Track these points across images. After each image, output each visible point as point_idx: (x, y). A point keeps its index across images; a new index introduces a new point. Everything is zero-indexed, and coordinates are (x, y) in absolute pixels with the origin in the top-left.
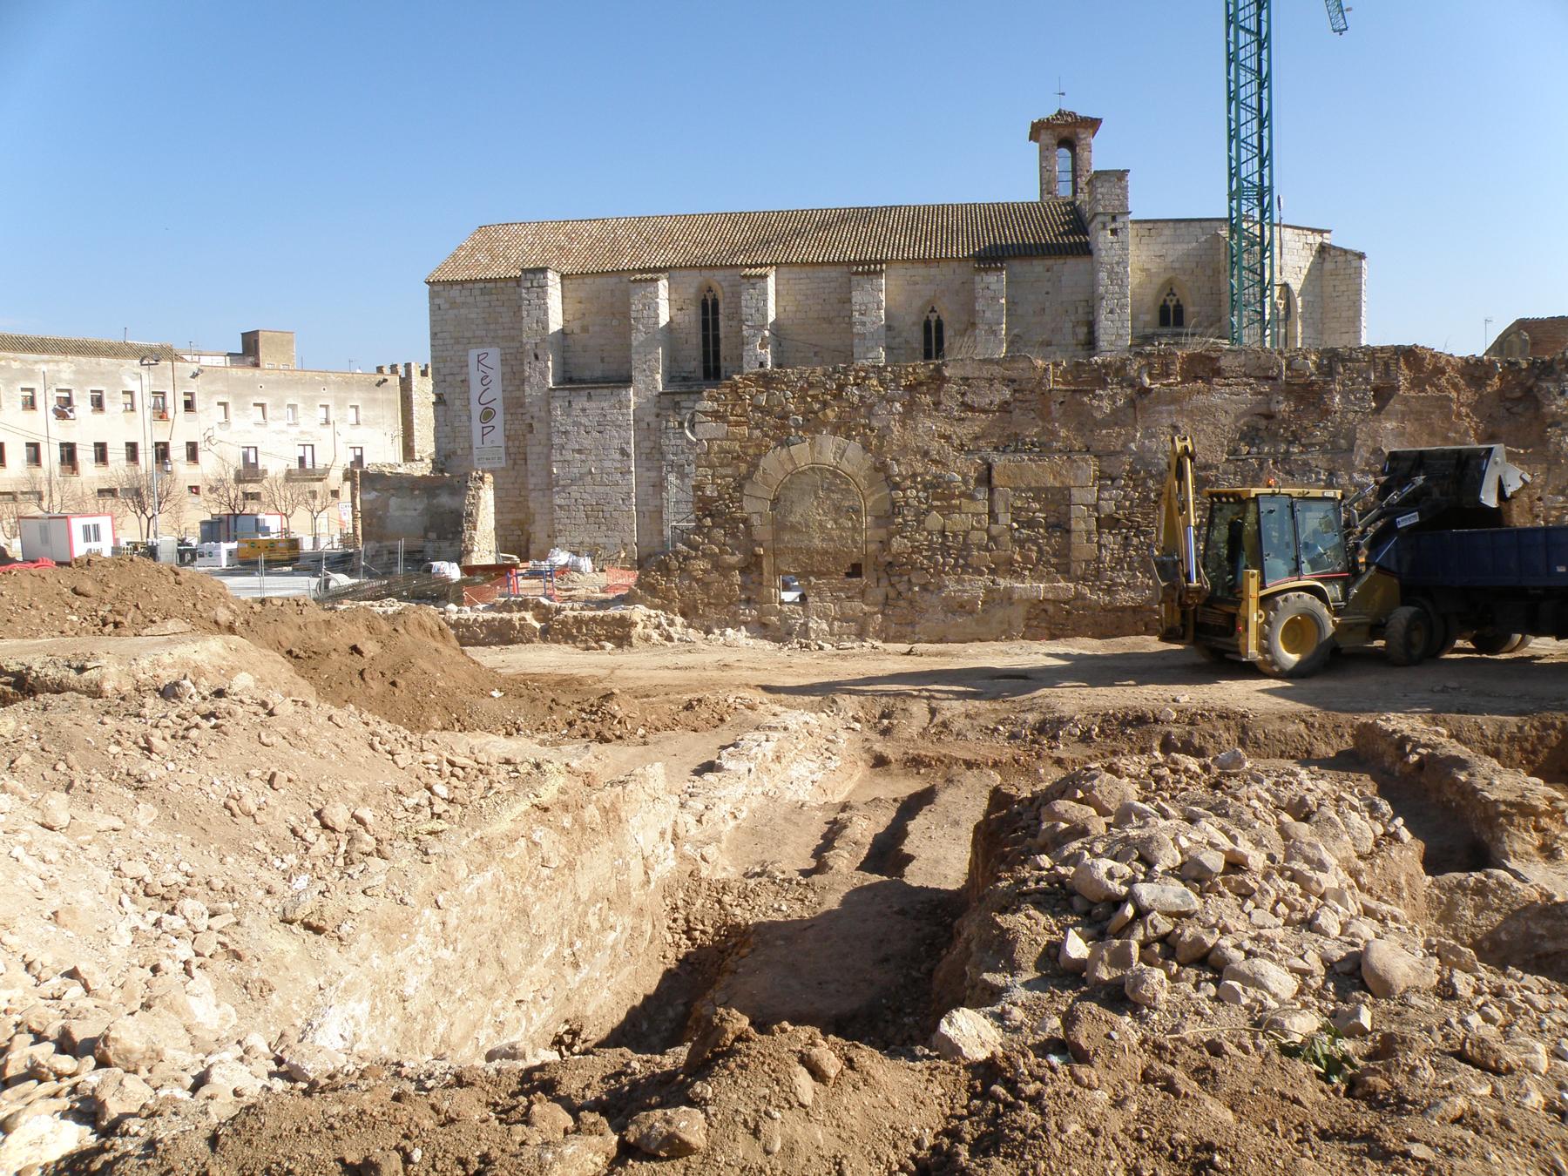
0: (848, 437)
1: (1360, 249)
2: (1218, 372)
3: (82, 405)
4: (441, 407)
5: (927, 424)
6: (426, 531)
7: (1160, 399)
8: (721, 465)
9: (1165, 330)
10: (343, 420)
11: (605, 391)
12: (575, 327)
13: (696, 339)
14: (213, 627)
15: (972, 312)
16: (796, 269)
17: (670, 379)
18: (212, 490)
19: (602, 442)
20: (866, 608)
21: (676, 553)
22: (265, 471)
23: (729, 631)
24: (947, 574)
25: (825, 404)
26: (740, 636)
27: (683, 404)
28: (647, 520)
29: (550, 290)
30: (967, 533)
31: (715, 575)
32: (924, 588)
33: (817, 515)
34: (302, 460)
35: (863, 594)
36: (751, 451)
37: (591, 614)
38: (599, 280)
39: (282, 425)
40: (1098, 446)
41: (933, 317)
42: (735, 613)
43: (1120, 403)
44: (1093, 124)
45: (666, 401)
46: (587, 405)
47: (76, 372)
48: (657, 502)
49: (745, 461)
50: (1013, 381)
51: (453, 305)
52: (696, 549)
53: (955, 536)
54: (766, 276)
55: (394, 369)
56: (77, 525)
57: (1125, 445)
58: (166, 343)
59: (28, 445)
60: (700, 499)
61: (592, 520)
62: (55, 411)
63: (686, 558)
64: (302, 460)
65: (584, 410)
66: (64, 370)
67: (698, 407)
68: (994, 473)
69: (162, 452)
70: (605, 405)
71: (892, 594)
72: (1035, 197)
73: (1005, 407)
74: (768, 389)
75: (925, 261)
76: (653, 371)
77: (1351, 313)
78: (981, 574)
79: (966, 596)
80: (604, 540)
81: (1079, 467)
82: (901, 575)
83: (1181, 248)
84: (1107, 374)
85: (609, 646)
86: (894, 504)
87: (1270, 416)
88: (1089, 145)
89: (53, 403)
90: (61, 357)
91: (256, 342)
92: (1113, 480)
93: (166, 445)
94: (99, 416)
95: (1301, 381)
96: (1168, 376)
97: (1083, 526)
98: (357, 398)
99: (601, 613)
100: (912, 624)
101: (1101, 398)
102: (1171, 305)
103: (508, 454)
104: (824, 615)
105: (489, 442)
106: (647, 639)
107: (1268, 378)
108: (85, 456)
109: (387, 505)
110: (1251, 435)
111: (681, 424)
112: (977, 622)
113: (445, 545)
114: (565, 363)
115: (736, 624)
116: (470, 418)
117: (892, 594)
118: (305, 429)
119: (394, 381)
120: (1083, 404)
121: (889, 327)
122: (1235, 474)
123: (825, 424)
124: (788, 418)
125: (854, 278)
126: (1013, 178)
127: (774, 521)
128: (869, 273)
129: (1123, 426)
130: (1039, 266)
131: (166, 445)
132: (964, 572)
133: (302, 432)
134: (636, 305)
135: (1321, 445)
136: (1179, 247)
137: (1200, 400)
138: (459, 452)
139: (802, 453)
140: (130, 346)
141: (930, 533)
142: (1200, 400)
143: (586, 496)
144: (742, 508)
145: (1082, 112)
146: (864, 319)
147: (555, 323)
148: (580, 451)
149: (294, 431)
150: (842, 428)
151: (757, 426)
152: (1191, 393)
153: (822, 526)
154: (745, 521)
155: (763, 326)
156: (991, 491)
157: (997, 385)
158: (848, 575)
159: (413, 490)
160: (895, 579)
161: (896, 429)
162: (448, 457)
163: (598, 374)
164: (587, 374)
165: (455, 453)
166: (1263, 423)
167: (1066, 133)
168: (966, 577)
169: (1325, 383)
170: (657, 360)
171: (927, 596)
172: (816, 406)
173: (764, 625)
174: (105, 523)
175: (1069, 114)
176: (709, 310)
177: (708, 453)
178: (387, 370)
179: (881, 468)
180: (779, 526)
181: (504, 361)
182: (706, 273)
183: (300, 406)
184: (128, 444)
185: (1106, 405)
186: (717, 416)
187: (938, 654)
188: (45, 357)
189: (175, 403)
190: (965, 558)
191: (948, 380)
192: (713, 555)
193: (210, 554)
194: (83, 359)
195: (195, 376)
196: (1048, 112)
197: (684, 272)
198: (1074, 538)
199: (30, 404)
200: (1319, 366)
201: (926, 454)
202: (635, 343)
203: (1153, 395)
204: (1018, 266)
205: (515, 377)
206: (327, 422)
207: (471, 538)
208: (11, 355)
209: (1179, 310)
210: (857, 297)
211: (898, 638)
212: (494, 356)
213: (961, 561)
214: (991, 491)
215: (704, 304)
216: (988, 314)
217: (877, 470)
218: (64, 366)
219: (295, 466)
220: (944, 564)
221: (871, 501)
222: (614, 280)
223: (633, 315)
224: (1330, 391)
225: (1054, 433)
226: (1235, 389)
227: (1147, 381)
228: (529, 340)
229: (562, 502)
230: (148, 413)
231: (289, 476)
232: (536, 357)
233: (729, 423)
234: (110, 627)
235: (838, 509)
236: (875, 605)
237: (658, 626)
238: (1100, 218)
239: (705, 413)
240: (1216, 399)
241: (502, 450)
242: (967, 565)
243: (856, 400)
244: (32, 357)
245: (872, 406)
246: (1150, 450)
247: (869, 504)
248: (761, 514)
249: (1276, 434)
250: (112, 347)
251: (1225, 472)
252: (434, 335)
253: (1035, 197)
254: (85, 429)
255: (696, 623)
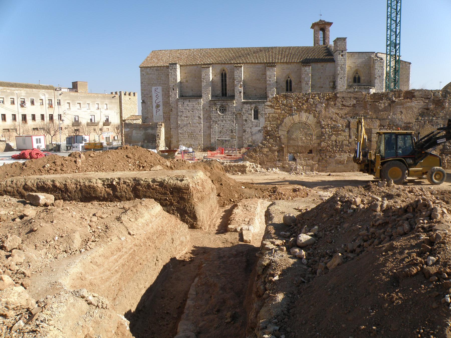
0: (309, 113)
1: (409, 61)
2: (414, 96)
3: (28, 103)
4: (144, 104)
5: (333, 110)
6: (144, 140)
7: (398, 104)
8: (273, 121)
9: (355, 84)
10: (103, 108)
11: (194, 100)
12: (184, 81)
13: (220, 85)
14: (167, 168)
15: (300, 78)
16: (249, 65)
17: (212, 96)
18: (65, 128)
19: (193, 114)
20: (313, 163)
21: (259, 146)
22: (111, 123)
23: (274, 169)
24: (337, 153)
25: (303, 104)
26: (277, 170)
27: (217, 104)
28: (206, 137)
29: (177, 70)
30: (343, 141)
31: (270, 153)
32: (330, 157)
33: (300, 136)
34: (91, 120)
35: (312, 158)
36: (281, 117)
37: (233, 164)
38: (191, 67)
39: (85, 109)
40: (380, 117)
41: (289, 79)
42: (275, 164)
43: (386, 105)
44: (330, 24)
45: (212, 102)
46: (188, 103)
47: (27, 93)
48: (209, 132)
49: (279, 120)
50: (357, 98)
51: (147, 73)
52: (265, 145)
53: (339, 142)
54: (242, 67)
55: (116, 93)
56: (34, 138)
57: (387, 117)
58: (52, 85)
59: (13, 115)
60: (266, 131)
61: (190, 137)
62: (20, 105)
63: (262, 148)
64: (91, 120)
65: (188, 105)
66: (23, 92)
67: (266, 104)
68: (351, 124)
69: (51, 117)
70: (194, 103)
71: (321, 159)
72: (311, 44)
73: (354, 105)
74: (286, 99)
75: (287, 63)
76: (208, 94)
77: (406, 80)
78: (346, 153)
79: (342, 159)
80: (193, 143)
81: (374, 123)
82: (323, 153)
83: (360, 60)
84: (383, 97)
85: (240, 173)
86: (322, 133)
87: (428, 109)
88: (329, 30)
89: (19, 103)
90: (22, 89)
91: (77, 85)
92: (384, 127)
93: (52, 115)
94: (33, 106)
95: (437, 99)
96: (400, 97)
97: (375, 140)
98: (107, 101)
99: (236, 164)
100: (326, 167)
101: (381, 103)
102: (357, 77)
103: (164, 118)
104: (301, 165)
105: (158, 115)
106: (251, 171)
107: (428, 98)
108: (29, 118)
109: (132, 133)
110: (422, 115)
111: (216, 109)
112: (345, 166)
113: (150, 144)
114: (181, 91)
115: (276, 167)
116: (152, 107)
117: (321, 159)
118: (92, 110)
119: (117, 96)
120: (376, 105)
121: (276, 82)
122: (417, 125)
123: (303, 109)
124: (292, 108)
125: (267, 68)
126: (306, 39)
127: (288, 137)
128: (271, 66)
129: (387, 111)
130: (319, 65)
131: (52, 115)
132: (342, 152)
133: (91, 112)
134: (203, 75)
135: (442, 117)
136: (359, 60)
137: (409, 104)
138: (149, 117)
139: (296, 118)
140: (41, 86)
141: (332, 141)
142: (409, 104)
143: (188, 130)
144: (278, 133)
145: (327, 21)
146: (270, 79)
147: (179, 80)
148: (186, 117)
149: (89, 111)
150: (308, 111)
151: (283, 110)
152: (406, 102)
153: (301, 139)
154: (279, 137)
155: (241, 81)
156: (350, 129)
157: (352, 99)
158: (308, 153)
159: (140, 128)
160: (322, 154)
161: (323, 111)
162: (146, 118)
163: (191, 94)
164: (187, 95)
165: (148, 117)
166: (426, 111)
167: (322, 26)
168: (342, 154)
169: (444, 100)
170: (209, 91)
171: (331, 159)
172: (301, 104)
173: (284, 167)
174: (42, 138)
175: (323, 21)
176: (223, 76)
177: (269, 117)
178: (114, 93)
179: (319, 122)
180: (289, 139)
181: (163, 91)
182: (223, 65)
183: (91, 104)
184: (41, 115)
185: (383, 105)
186: (271, 106)
187: (337, 176)
188: (17, 89)
189: (55, 103)
190: (342, 148)
191: (338, 98)
192: (270, 147)
193: (76, 147)
194: (28, 90)
195: (60, 95)
196: (317, 20)
197: (216, 65)
198: (372, 143)
199: (13, 103)
200: (442, 95)
201: (332, 118)
202: (203, 86)
203: (396, 103)
204: (313, 65)
205: (166, 94)
206: (98, 109)
207: (159, 142)
208: (7, 88)
209: (359, 78)
210: (268, 73)
211: (322, 171)
212: (160, 89)
213: (341, 149)
214: (350, 129)
215: (222, 74)
216: (306, 79)
217: (317, 123)
218: (22, 91)
219: (89, 121)
220: (336, 150)
221: (315, 131)
222: (195, 67)
223: (202, 77)
224: (445, 102)
225: (368, 113)
226: (418, 101)
227: (394, 99)
228: (171, 84)
229: (181, 132)
230: (47, 106)
231: (88, 124)
232: (173, 89)
233: (275, 109)
234: (141, 168)
235: (306, 134)
236: (316, 161)
237: (253, 168)
238: (338, 52)
239: (268, 106)
240: (413, 104)
241: (162, 117)
242: (342, 150)
243: (312, 103)
244: (13, 89)
245: (316, 104)
246: (394, 118)
247: (315, 133)
248: (284, 135)
249: (429, 114)
250: (36, 86)
251: (415, 125)
252: (142, 83)
253: (313, 46)
254: (29, 110)
255: (264, 166)
